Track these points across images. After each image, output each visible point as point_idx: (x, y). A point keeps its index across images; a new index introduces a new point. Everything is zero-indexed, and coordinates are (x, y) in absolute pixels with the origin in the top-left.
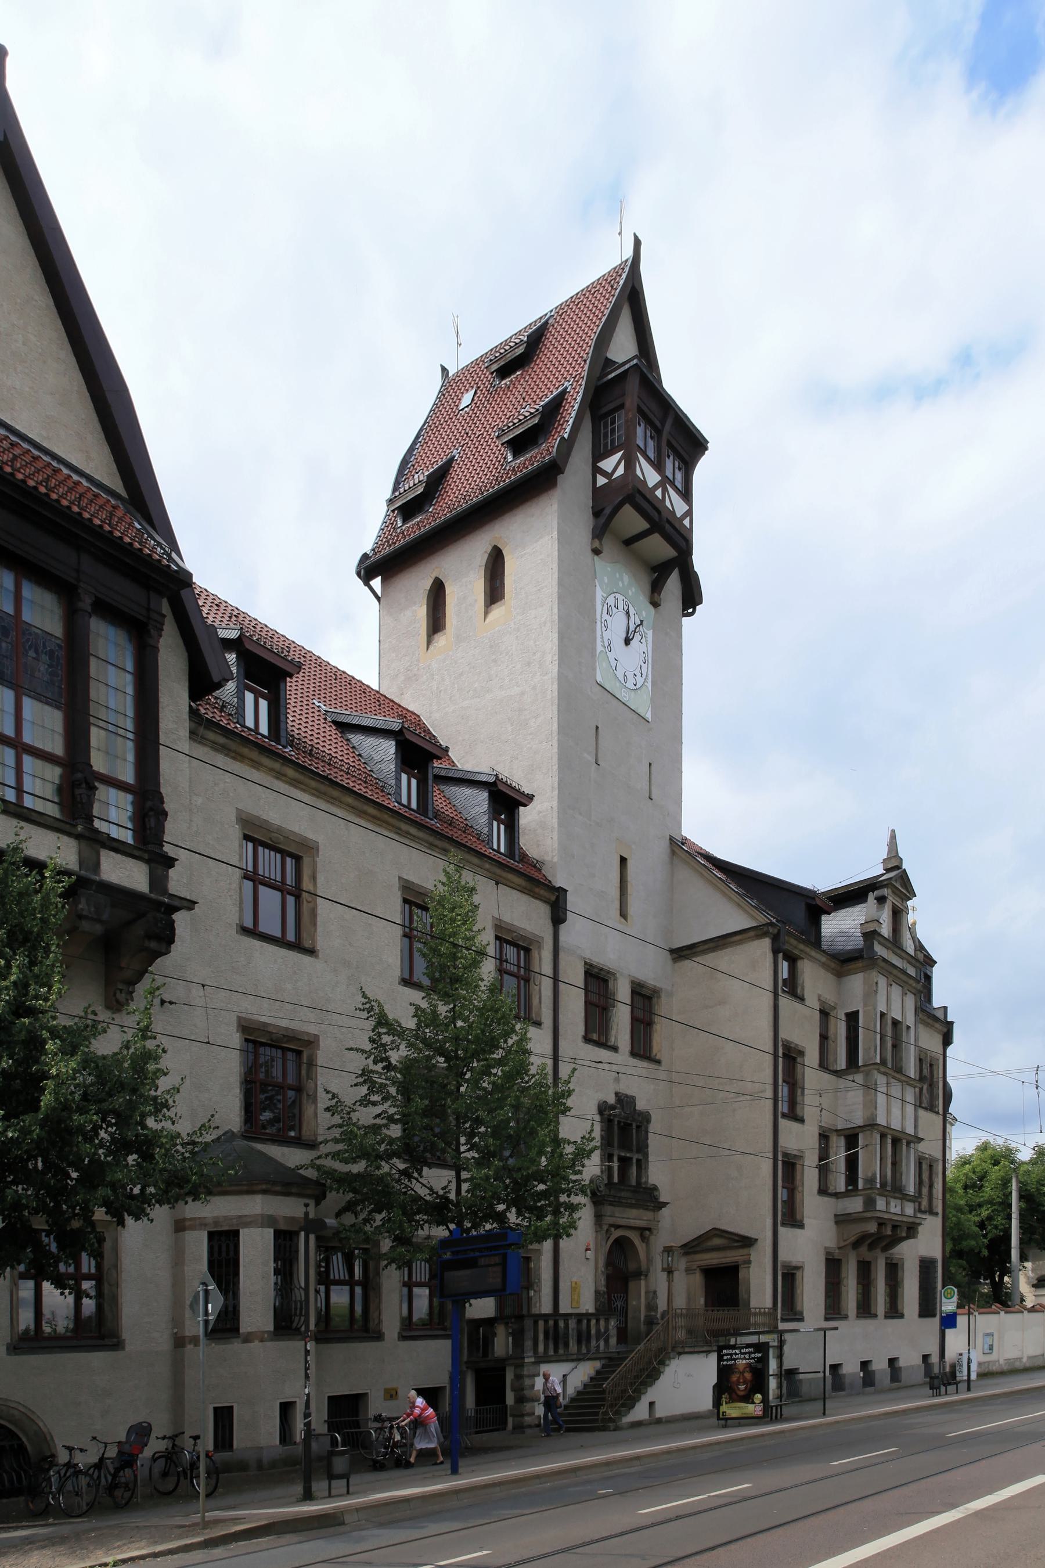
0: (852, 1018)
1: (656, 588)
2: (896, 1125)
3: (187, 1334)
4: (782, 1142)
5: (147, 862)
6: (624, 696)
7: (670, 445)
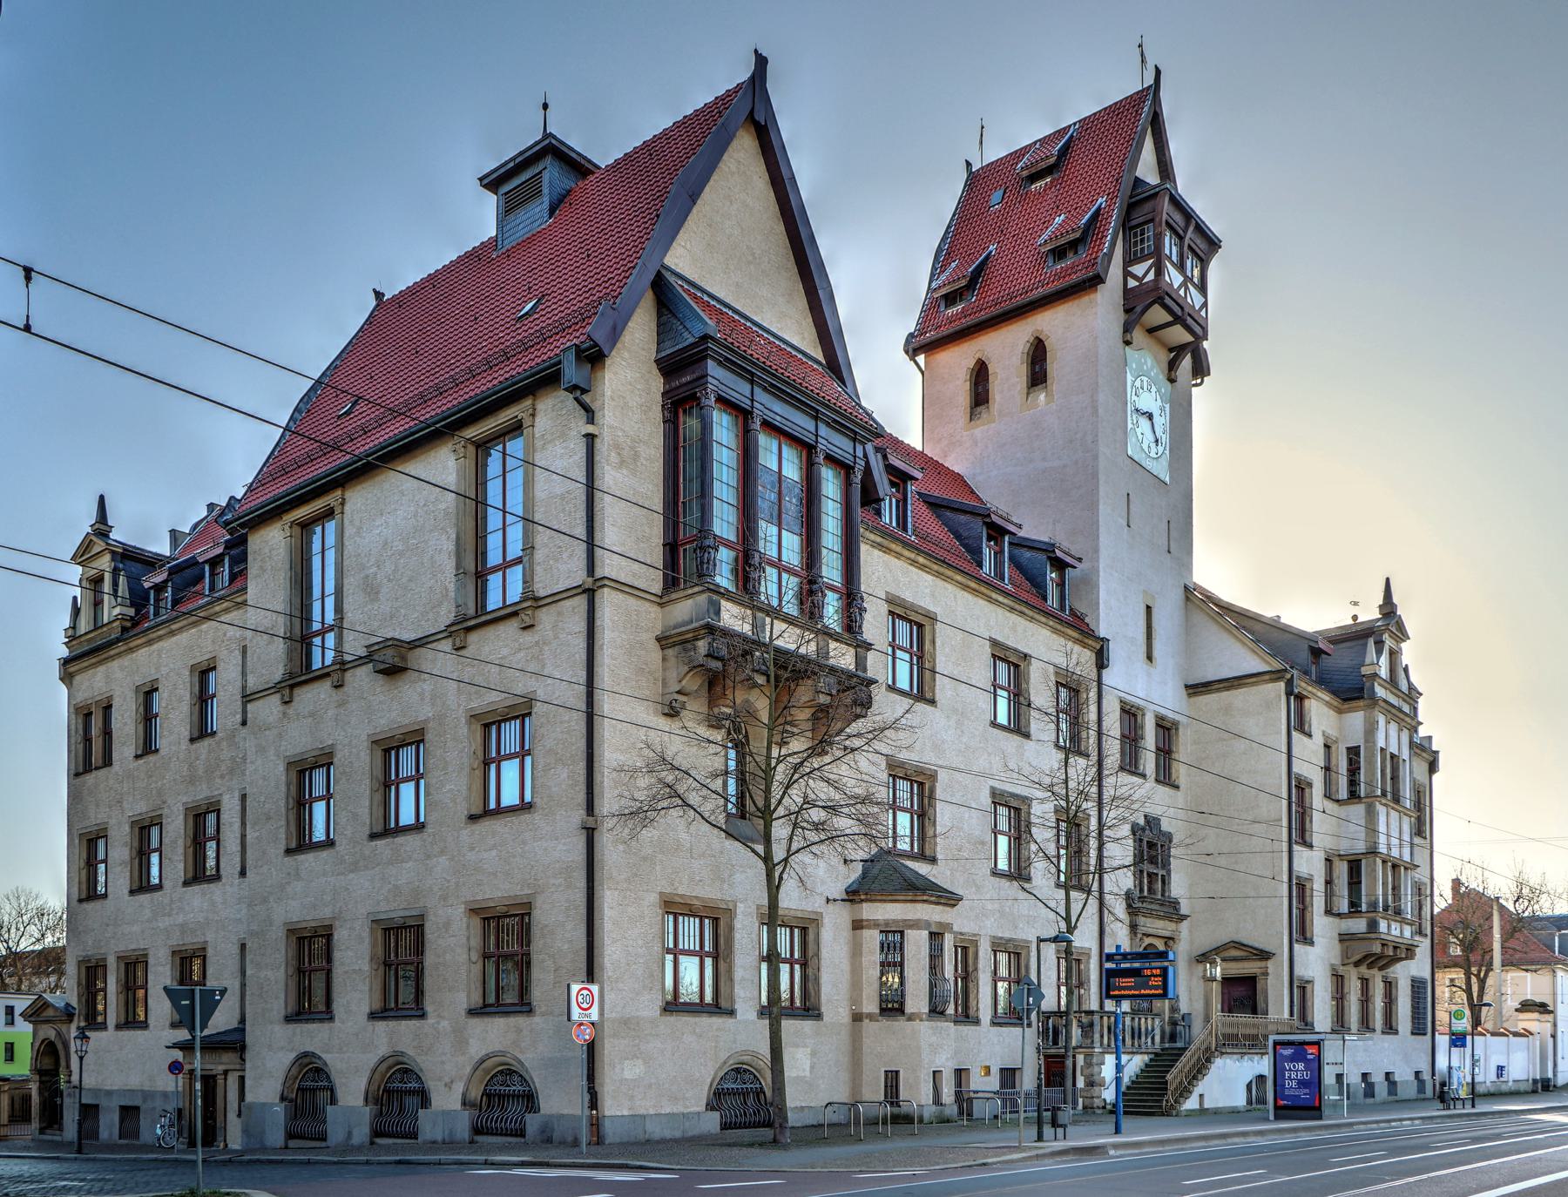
2: (1395, 853)
3: (865, 1011)
4: (1296, 867)
6: (1148, 464)
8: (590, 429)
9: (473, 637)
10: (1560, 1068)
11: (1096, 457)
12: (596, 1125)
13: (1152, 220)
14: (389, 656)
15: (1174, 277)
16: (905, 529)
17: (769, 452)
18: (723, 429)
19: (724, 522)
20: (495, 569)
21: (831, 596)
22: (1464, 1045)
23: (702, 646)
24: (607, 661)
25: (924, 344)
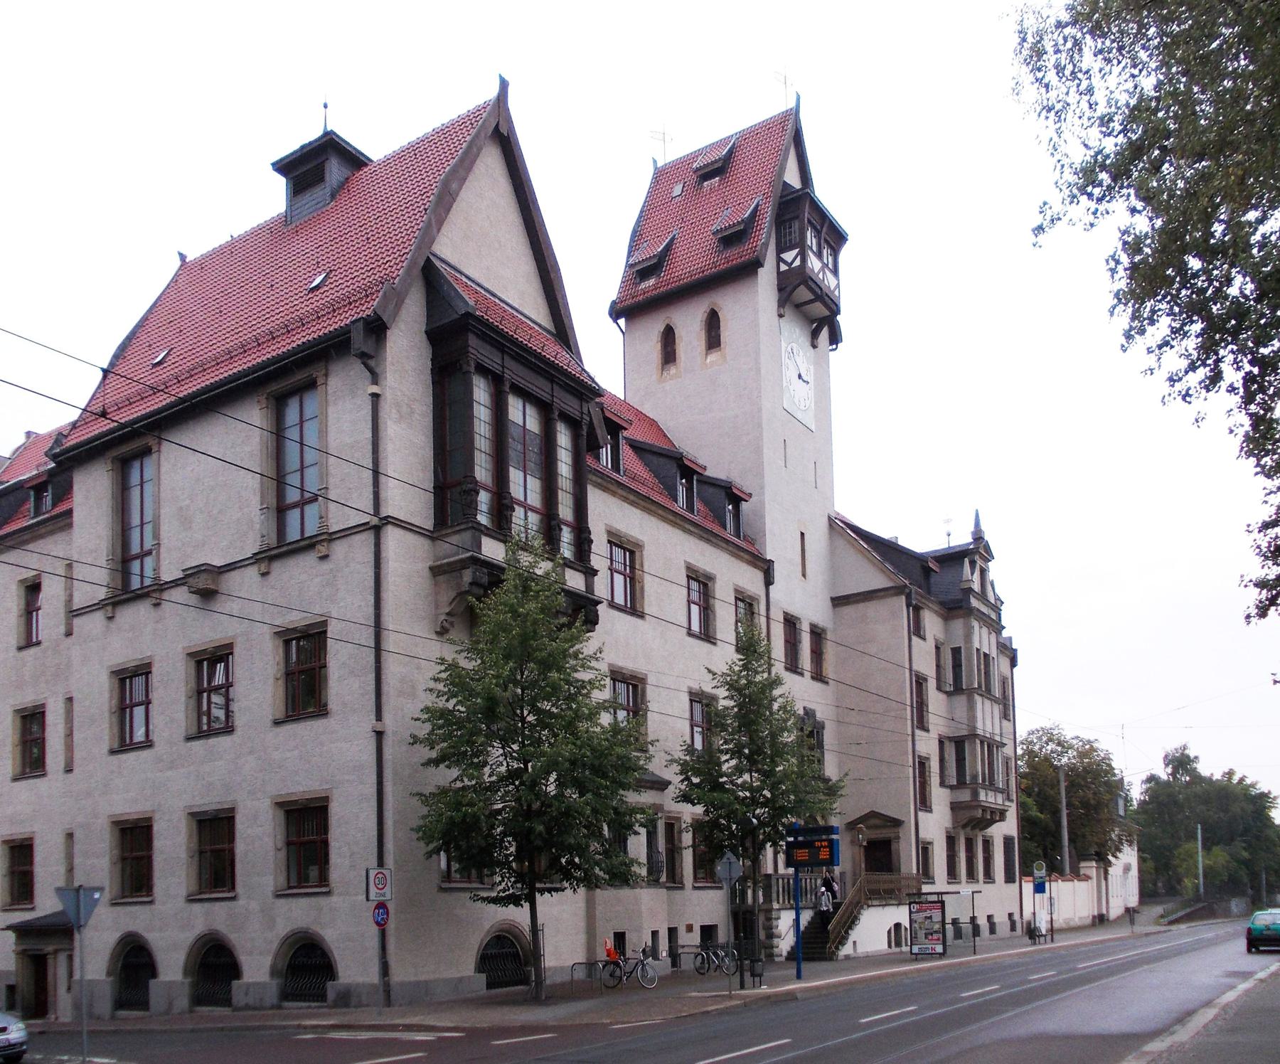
0: (956, 652)
1: (815, 335)
4: (917, 748)
5: (584, 573)
7: (826, 241)
8: (375, 389)
9: (277, 567)
10: (1111, 904)
11: (760, 410)
12: (387, 988)
13: (797, 217)
14: (203, 582)
15: (814, 263)
16: (618, 471)
17: (516, 410)
18: (481, 392)
19: (482, 471)
20: (295, 506)
21: (565, 532)
22: (1043, 891)
23: (467, 576)
24: (392, 588)
25: (627, 311)
